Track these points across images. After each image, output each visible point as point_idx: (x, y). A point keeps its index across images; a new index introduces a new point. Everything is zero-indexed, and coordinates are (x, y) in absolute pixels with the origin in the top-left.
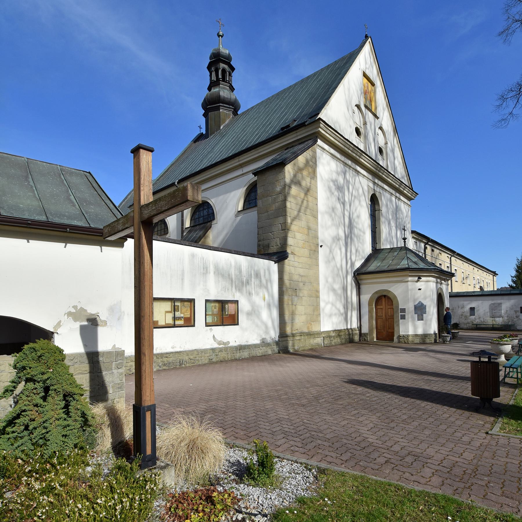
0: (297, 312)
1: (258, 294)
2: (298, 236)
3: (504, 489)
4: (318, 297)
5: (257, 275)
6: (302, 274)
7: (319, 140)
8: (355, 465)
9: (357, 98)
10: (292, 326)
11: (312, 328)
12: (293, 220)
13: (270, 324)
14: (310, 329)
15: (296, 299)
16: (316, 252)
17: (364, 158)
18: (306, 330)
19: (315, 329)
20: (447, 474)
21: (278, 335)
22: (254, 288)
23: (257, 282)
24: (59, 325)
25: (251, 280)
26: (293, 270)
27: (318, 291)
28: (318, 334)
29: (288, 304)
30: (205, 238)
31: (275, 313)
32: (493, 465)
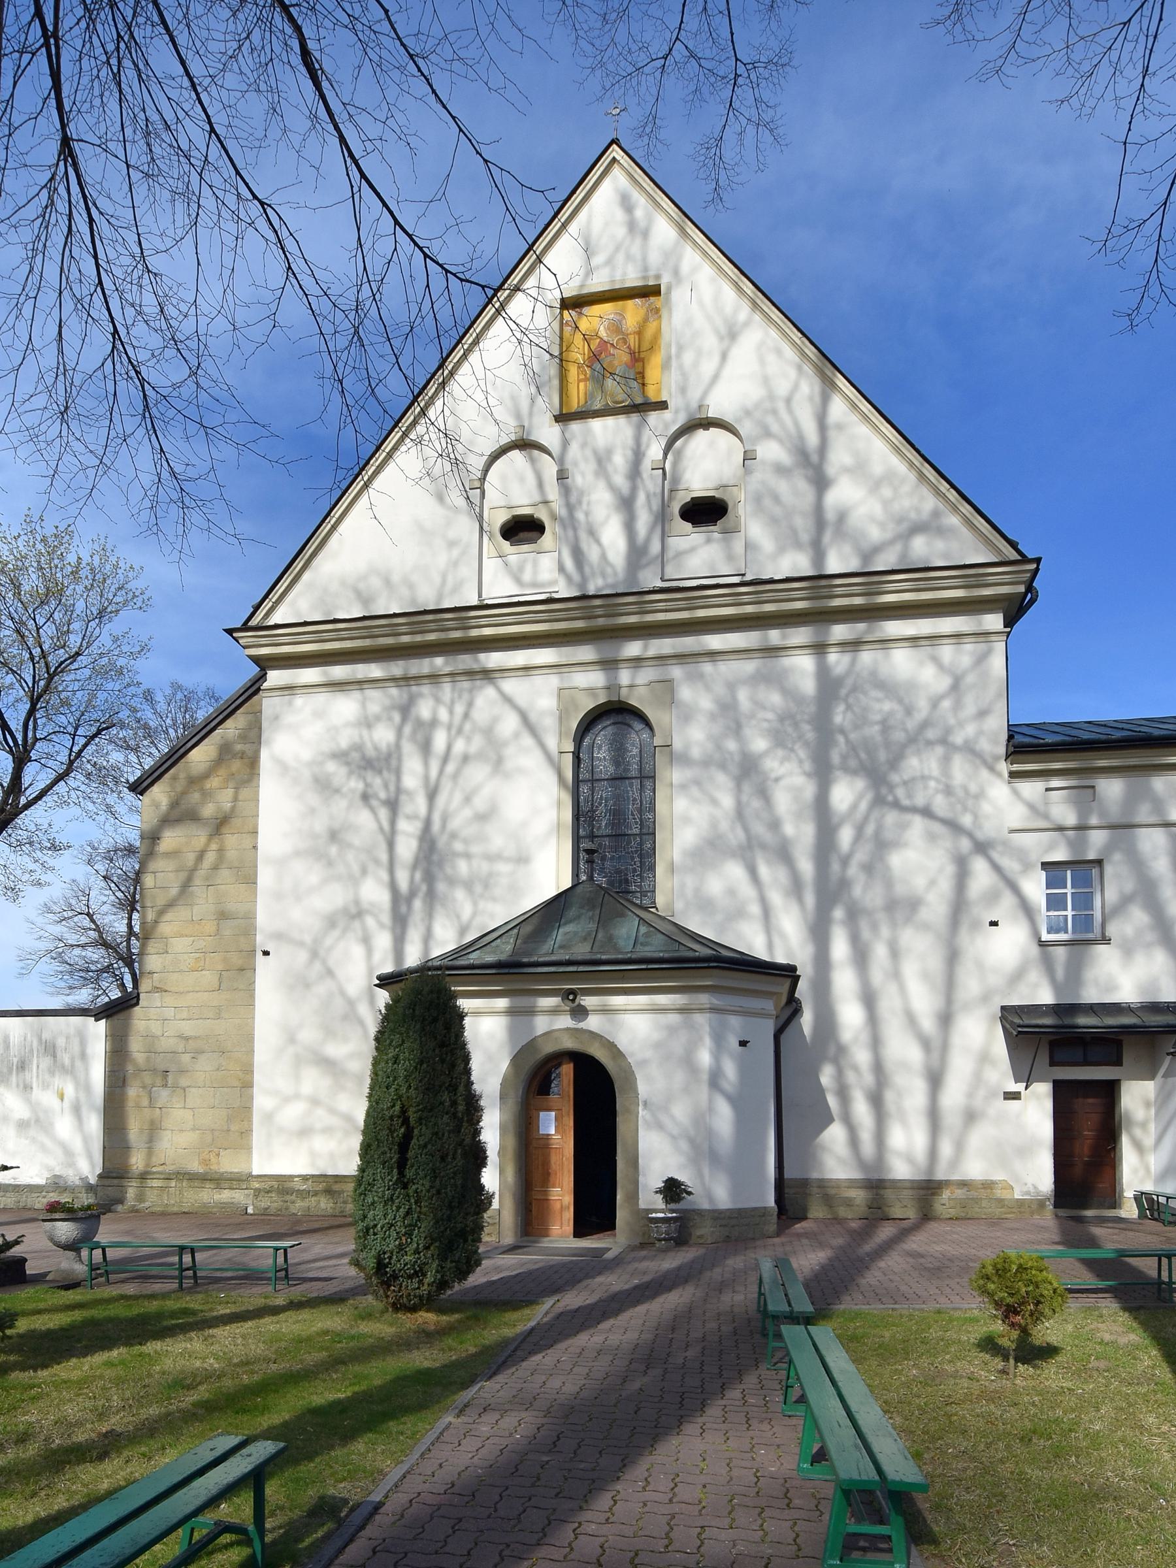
0: (164, 1125)
1: (45, 1086)
2: (179, 945)
3: (757, 1490)
4: (248, 1085)
5: (50, 1049)
6: (188, 1033)
7: (464, 1004)
8: (449, 1540)
9: (494, 553)
10: (150, 1151)
11: (218, 1163)
12: (161, 913)
13: (77, 1145)
14: (214, 1167)
15: (163, 1095)
16: (246, 970)
17: (483, 621)
18: (195, 1167)
19: (228, 1164)
20: (787, 1511)
21: (99, 1170)
22: (38, 1076)
23: (46, 1062)
24: (3, 1235)
25: (31, 1061)
26: (155, 1028)
27: (248, 1069)
28: (240, 1180)
29: (138, 1106)
30: (476, 1318)
31: (94, 1124)
32: (788, 1505)
